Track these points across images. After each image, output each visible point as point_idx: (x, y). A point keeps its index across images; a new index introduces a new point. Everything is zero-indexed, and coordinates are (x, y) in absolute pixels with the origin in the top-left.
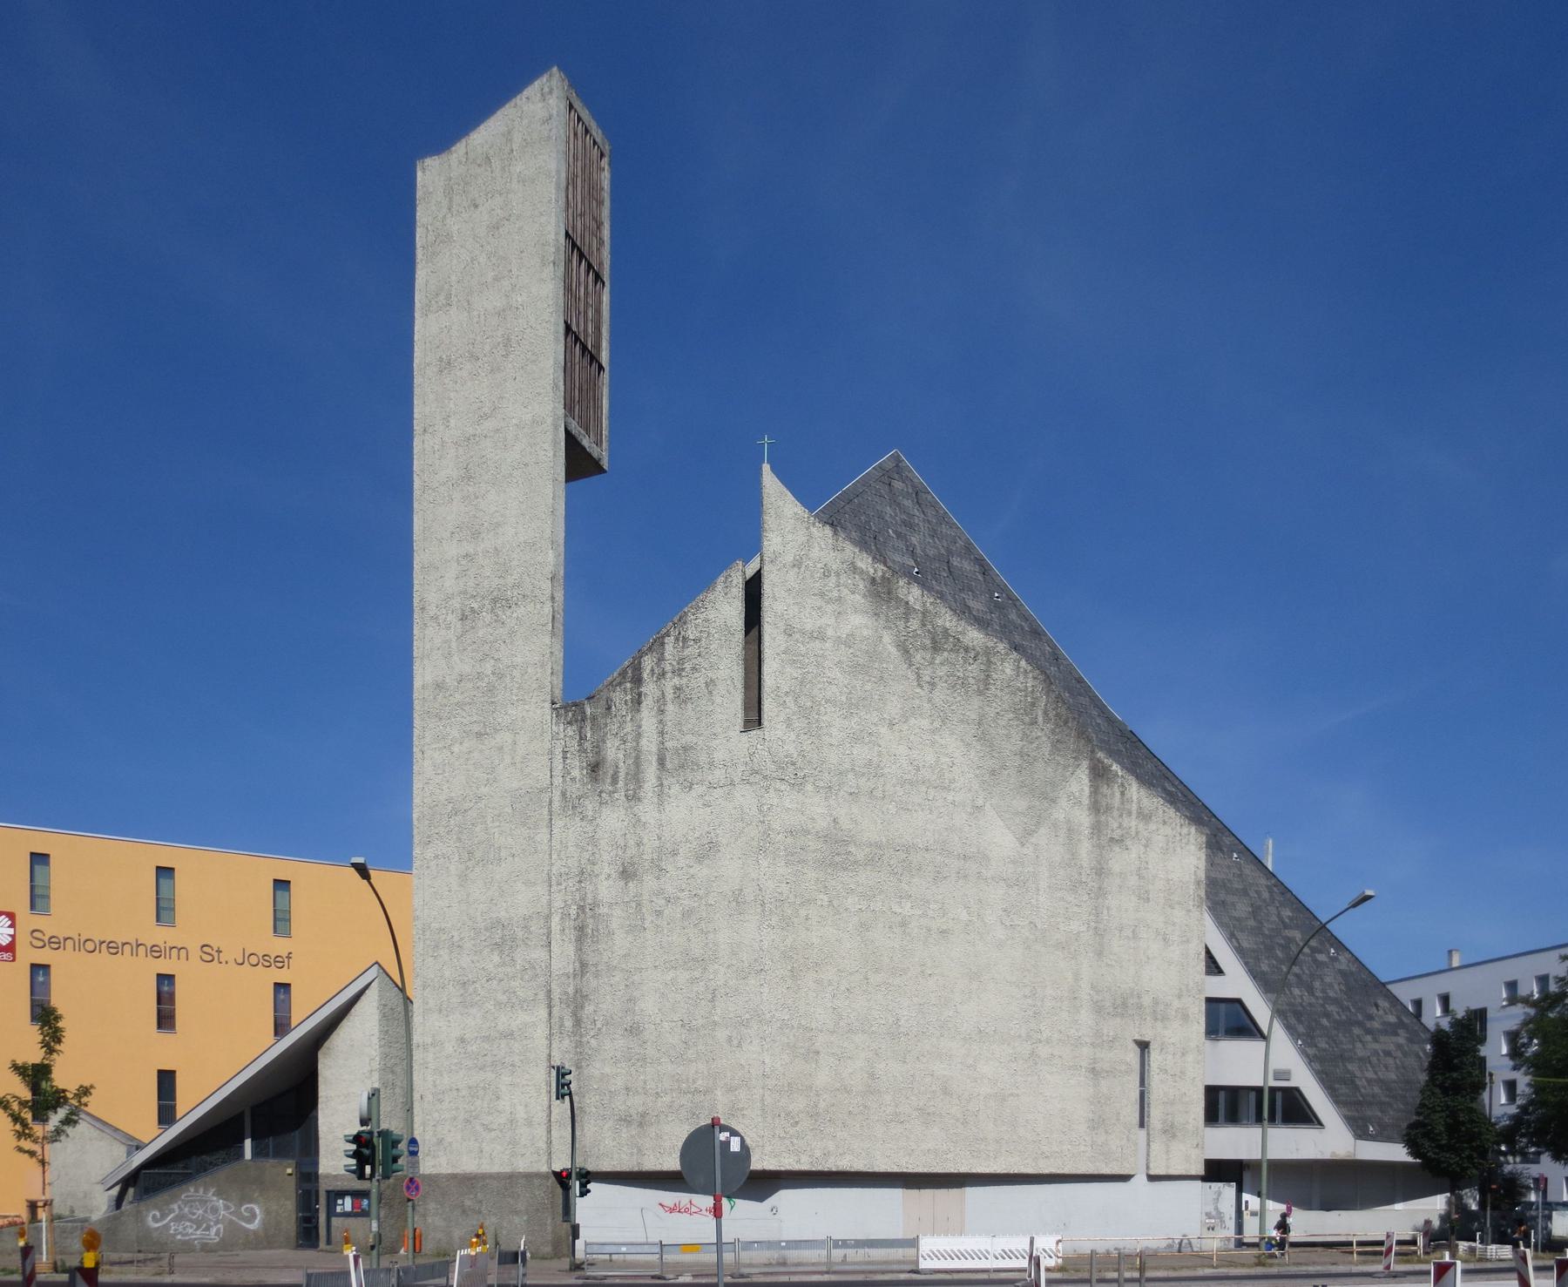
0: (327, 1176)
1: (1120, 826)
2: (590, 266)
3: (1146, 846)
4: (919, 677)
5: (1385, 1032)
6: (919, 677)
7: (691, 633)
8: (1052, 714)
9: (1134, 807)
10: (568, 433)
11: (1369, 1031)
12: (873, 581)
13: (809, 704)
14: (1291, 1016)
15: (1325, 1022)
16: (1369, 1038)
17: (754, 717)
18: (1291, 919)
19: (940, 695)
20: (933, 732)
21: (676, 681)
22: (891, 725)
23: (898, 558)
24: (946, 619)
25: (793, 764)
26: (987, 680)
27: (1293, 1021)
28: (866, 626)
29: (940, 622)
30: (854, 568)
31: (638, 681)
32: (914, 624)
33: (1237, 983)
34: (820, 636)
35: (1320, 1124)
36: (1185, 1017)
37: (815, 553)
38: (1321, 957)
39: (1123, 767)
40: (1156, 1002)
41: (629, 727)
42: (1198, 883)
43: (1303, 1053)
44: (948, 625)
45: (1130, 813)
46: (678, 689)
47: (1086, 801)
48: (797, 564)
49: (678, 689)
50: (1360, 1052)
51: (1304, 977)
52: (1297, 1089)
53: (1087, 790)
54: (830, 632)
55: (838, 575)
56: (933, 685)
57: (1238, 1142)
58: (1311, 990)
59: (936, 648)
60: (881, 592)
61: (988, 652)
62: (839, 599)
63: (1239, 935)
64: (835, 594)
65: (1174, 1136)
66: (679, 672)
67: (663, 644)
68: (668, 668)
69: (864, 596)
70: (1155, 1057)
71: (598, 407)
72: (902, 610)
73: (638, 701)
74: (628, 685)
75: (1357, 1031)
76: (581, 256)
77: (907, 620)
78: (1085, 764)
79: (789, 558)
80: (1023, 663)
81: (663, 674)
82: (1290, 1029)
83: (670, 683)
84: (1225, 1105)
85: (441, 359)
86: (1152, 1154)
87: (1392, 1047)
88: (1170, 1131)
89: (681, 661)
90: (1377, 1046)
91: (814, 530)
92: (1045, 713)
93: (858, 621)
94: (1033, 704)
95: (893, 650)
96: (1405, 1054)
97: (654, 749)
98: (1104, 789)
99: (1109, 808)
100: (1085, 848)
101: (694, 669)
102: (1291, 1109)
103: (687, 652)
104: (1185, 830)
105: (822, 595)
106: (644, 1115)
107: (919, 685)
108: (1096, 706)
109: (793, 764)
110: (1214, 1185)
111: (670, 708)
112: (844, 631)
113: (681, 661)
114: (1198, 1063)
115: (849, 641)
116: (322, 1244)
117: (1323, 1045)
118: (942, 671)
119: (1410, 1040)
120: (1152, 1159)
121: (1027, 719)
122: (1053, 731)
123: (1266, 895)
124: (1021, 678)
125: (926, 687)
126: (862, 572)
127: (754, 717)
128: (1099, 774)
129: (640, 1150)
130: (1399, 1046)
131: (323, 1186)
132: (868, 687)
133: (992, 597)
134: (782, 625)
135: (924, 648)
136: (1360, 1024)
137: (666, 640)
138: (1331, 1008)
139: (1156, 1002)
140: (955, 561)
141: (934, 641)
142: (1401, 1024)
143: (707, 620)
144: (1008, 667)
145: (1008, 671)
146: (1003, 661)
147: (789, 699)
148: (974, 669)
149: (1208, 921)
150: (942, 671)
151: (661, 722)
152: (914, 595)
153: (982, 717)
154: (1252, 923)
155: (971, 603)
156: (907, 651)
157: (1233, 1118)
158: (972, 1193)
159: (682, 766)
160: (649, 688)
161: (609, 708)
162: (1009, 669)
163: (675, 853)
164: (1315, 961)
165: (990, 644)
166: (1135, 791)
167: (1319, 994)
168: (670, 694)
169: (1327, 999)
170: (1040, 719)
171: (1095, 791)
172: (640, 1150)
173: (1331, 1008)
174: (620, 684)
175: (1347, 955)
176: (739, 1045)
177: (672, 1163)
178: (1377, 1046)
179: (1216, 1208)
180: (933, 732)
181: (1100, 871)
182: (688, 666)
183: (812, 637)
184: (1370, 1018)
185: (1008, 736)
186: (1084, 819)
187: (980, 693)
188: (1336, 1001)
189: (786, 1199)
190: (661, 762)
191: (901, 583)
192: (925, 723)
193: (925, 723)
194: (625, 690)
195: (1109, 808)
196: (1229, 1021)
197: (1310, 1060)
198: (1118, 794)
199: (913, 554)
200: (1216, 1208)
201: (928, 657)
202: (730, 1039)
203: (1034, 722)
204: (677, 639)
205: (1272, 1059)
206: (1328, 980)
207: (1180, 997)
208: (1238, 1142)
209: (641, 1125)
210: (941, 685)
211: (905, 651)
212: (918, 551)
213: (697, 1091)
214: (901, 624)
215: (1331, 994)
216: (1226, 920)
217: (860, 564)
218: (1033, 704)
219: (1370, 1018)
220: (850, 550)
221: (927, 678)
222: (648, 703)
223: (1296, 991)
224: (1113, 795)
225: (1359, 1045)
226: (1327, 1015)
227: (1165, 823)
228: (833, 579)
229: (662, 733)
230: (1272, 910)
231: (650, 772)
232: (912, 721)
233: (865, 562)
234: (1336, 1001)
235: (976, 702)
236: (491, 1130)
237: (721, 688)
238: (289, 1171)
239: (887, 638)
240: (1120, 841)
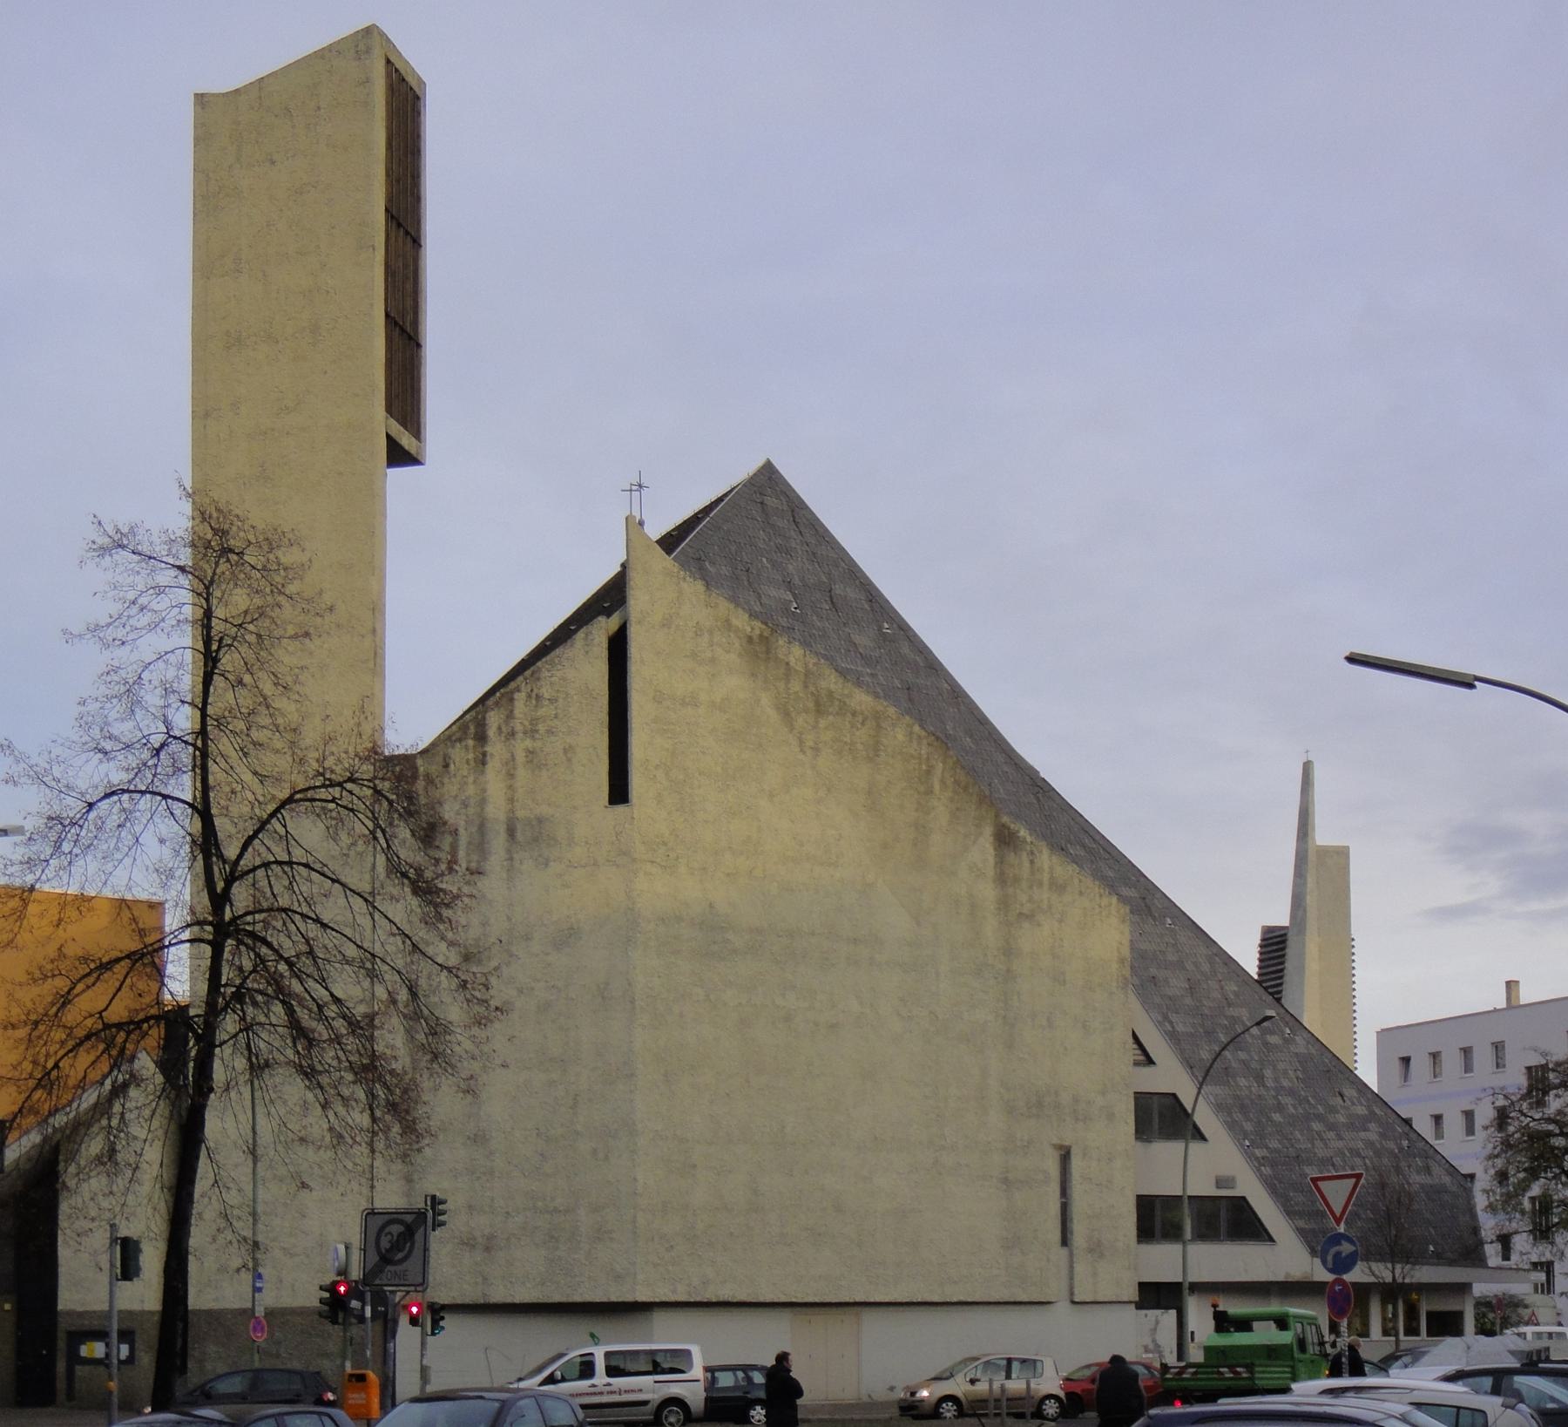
0: (71, 1313)
1: (1030, 900)
2: (407, 233)
3: (1060, 921)
5: (1351, 1126)
6: (801, 742)
7: (546, 692)
8: (950, 781)
9: (1046, 877)
10: (388, 436)
11: (1332, 1127)
12: (750, 640)
14: (1235, 1113)
15: (1277, 1117)
16: (1331, 1135)
17: (619, 792)
18: (1236, 994)
21: (528, 743)
22: (771, 796)
23: (773, 592)
24: (831, 681)
25: (665, 844)
26: (875, 748)
27: (1238, 1116)
29: (823, 684)
31: (481, 738)
32: (796, 686)
33: (1170, 1077)
34: (691, 701)
35: (1271, 1239)
36: (1111, 1117)
38: (1274, 1039)
39: (1032, 830)
40: (1076, 1100)
41: (471, 790)
42: (1122, 961)
43: (1249, 1155)
44: (832, 687)
45: (1041, 884)
46: (530, 753)
47: (990, 872)
48: (666, 623)
49: (530, 753)
50: (1321, 1152)
51: (1254, 1065)
52: (1244, 1198)
53: (991, 860)
55: (711, 632)
56: (816, 750)
57: (1163, 1262)
58: (1260, 1078)
59: (820, 710)
60: (759, 651)
61: (877, 716)
62: (713, 660)
63: (1173, 1017)
64: (709, 654)
65: (1102, 1256)
66: (532, 732)
67: (512, 700)
68: (519, 728)
69: (740, 655)
70: (1076, 1163)
72: (782, 670)
73: (482, 761)
74: (471, 742)
75: (1316, 1126)
76: (399, 225)
77: (788, 681)
78: (988, 831)
80: (917, 728)
81: (513, 734)
82: (1232, 1126)
83: (521, 745)
84: (1156, 1218)
85: (228, 333)
86: (1077, 1279)
87: (1361, 1145)
88: (1097, 1249)
89: (534, 721)
90: (1340, 1144)
91: (685, 585)
92: (943, 782)
93: (734, 683)
94: (928, 772)
95: (773, 715)
96: (1378, 1153)
97: (502, 817)
98: (1011, 858)
99: (1017, 880)
100: (990, 928)
101: (550, 732)
102: (1233, 1220)
103: (541, 712)
104: (1105, 901)
106: (491, 1238)
108: (1004, 751)
109: (665, 844)
110: (1151, 1313)
111: (522, 773)
113: (534, 721)
114: (1126, 1168)
116: (61, 1396)
117: (1274, 1144)
119: (1383, 1135)
120: (1076, 1283)
121: (922, 789)
122: (951, 800)
123: (1206, 967)
125: (809, 752)
126: (737, 630)
127: (619, 792)
128: (1005, 839)
129: (485, 1279)
130: (1370, 1144)
131: (63, 1325)
133: (880, 628)
135: (806, 711)
136: (1319, 1117)
137: (516, 696)
138: (1287, 1100)
139: (1076, 1100)
140: (838, 589)
141: (817, 704)
142: (1372, 1116)
143: (564, 679)
146: (894, 725)
149: (1135, 1003)
151: (510, 787)
152: (796, 654)
154: (1188, 1001)
155: (857, 638)
157: (1172, 1233)
158: (870, 1318)
159: (536, 840)
160: (496, 748)
161: (446, 766)
162: (900, 736)
163: (528, 938)
164: (1266, 1044)
165: (880, 708)
166: (1046, 858)
167: (1270, 1083)
169: (1280, 1089)
170: (937, 786)
171: (1000, 861)
172: (485, 1279)
173: (1287, 1100)
174: (460, 740)
175: (1305, 1035)
176: (606, 1158)
177: (1173, 1313)
178: (1340, 1144)
179: (1154, 1341)
181: (1009, 951)
182: (541, 728)
183: (684, 703)
184: (1333, 1110)
186: (988, 892)
188: (1292, 1092)
189: (660, 1319)
190: (511, 832)
191: (781, 642)
194: (466, 747)
195: (1017, 880)
196: (1162, 1118)
197: (1257, 1163)
198: (1027, 864)
199: (789, 585)
200: (1154, 1341)
202: (595, 1152)
203: (929, 792)
204: (529, 696)
205: (1214, 1163)
206: (1281, 1066)
207: (1103, 1093)
208: (1163, 1262)
209: (488, 1249)
211: (786, 715)
212: (797, 581)
213: (556, 1210)
214: (781, 685)
215: (1285, 1083)
216: (1158, 1000)
217: (735, 622)
219: (1333, 1110)
220: (724, 606)
221: (810, 743)
222: (493, 765)
223: (1242, 1082)
224: (1020, 863)
225: (1318, 1143)
226: (1280, 1108)
227: (1081, 893)
229: (511, 800)
230: (1213, 984)
231: (498, 843)
233: (741, 620)
234: (1292, 1092)
236: (292, 1255)
238: (7, 1307)
239: (766, 699)
240: (1030, 917)
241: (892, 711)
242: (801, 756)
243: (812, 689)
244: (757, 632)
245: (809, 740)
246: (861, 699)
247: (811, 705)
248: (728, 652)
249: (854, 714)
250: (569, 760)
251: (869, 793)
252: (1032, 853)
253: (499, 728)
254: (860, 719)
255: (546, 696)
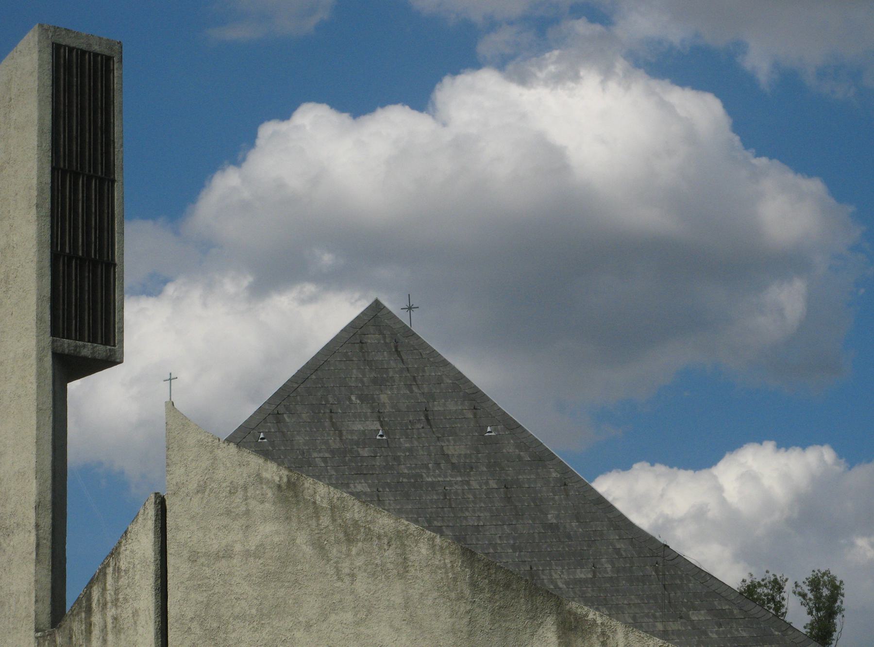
4: (338, 571)
6: (338, 571)
12: (279, 486)
13: (215, 625)
19: (361, 586)
20: (357, 624)
22: (308, 627)
24: (356, 511)
26: (404, 564)
28: (277, 533)
29: (348, 515)
30: (259, 478)
31: (89, 610)
32: (325, 521)
34: (227, 554)
37: (220, 474)
44: (356, 516)
46: (115, 619)
48: (201, 489)
54: (238, 547)
56: (353, 576)
59: (350, 540)
60: (289, 493)
61: (400, 536)
64: (243, 508)
69: (274, 503)
71: (78, 242)
72: (311, 510)
73: (89, 631)
77: (318, 518)
79: (193, 486)
80: (438, 540)
95: (308, 550)
105: (228, 512)
107: (340, 579)
111: (110, 637)
112: (253, 543)
115: (258, 552)
118: (359, 562)
121: (453, 595)
124: (438, 556)
125: (347, 580)
126: (268, 482)
132: (281, 592)
133: (483, 429)
134: (186, 554)
135: (338, 542)
141: (346, 534)
143: (132, 551)
144: (424, 549)
145: (424, 551)
146: (417, 542)
147: (195, 625)
148: (390, 554)
150: (359, 562)
152: (321, 492)
153: (407, 600)
155: (450, 450)
156: (322, 548)
168: (109, 621)
180: (357, 624)
183: (218, 557)
185: (437, 616)
187: (401, 576)
191: (307, 485)
192: (349, 617)
193: (349, 617)
201: (344, 549)
210: (361, 576)
211: (320, 547)
214: (313, 523)
217: (266, 475)
218: (455, 579)
221: (347, 571)
222: (96, 632)
228: (240, 494)
232: (333, 618)
235: (398, 586)
237: (142, 619)
239: (302, 539)
241: (413, 527)
242: (339, 584)
243: (339, 521)
244: (285, 480)
245: (345, 567)
246: (385, 522)
247: (341, 536)
248: (262, 502)
249: (379, 537)
250: (135, 623)
251: (406, 607)
252: (603, 634)
253: (98, 600)
254: (386, 541)
255: (123, 568)
